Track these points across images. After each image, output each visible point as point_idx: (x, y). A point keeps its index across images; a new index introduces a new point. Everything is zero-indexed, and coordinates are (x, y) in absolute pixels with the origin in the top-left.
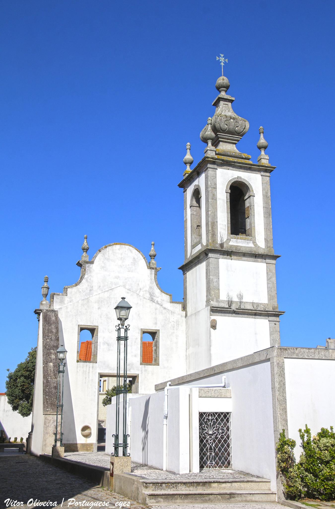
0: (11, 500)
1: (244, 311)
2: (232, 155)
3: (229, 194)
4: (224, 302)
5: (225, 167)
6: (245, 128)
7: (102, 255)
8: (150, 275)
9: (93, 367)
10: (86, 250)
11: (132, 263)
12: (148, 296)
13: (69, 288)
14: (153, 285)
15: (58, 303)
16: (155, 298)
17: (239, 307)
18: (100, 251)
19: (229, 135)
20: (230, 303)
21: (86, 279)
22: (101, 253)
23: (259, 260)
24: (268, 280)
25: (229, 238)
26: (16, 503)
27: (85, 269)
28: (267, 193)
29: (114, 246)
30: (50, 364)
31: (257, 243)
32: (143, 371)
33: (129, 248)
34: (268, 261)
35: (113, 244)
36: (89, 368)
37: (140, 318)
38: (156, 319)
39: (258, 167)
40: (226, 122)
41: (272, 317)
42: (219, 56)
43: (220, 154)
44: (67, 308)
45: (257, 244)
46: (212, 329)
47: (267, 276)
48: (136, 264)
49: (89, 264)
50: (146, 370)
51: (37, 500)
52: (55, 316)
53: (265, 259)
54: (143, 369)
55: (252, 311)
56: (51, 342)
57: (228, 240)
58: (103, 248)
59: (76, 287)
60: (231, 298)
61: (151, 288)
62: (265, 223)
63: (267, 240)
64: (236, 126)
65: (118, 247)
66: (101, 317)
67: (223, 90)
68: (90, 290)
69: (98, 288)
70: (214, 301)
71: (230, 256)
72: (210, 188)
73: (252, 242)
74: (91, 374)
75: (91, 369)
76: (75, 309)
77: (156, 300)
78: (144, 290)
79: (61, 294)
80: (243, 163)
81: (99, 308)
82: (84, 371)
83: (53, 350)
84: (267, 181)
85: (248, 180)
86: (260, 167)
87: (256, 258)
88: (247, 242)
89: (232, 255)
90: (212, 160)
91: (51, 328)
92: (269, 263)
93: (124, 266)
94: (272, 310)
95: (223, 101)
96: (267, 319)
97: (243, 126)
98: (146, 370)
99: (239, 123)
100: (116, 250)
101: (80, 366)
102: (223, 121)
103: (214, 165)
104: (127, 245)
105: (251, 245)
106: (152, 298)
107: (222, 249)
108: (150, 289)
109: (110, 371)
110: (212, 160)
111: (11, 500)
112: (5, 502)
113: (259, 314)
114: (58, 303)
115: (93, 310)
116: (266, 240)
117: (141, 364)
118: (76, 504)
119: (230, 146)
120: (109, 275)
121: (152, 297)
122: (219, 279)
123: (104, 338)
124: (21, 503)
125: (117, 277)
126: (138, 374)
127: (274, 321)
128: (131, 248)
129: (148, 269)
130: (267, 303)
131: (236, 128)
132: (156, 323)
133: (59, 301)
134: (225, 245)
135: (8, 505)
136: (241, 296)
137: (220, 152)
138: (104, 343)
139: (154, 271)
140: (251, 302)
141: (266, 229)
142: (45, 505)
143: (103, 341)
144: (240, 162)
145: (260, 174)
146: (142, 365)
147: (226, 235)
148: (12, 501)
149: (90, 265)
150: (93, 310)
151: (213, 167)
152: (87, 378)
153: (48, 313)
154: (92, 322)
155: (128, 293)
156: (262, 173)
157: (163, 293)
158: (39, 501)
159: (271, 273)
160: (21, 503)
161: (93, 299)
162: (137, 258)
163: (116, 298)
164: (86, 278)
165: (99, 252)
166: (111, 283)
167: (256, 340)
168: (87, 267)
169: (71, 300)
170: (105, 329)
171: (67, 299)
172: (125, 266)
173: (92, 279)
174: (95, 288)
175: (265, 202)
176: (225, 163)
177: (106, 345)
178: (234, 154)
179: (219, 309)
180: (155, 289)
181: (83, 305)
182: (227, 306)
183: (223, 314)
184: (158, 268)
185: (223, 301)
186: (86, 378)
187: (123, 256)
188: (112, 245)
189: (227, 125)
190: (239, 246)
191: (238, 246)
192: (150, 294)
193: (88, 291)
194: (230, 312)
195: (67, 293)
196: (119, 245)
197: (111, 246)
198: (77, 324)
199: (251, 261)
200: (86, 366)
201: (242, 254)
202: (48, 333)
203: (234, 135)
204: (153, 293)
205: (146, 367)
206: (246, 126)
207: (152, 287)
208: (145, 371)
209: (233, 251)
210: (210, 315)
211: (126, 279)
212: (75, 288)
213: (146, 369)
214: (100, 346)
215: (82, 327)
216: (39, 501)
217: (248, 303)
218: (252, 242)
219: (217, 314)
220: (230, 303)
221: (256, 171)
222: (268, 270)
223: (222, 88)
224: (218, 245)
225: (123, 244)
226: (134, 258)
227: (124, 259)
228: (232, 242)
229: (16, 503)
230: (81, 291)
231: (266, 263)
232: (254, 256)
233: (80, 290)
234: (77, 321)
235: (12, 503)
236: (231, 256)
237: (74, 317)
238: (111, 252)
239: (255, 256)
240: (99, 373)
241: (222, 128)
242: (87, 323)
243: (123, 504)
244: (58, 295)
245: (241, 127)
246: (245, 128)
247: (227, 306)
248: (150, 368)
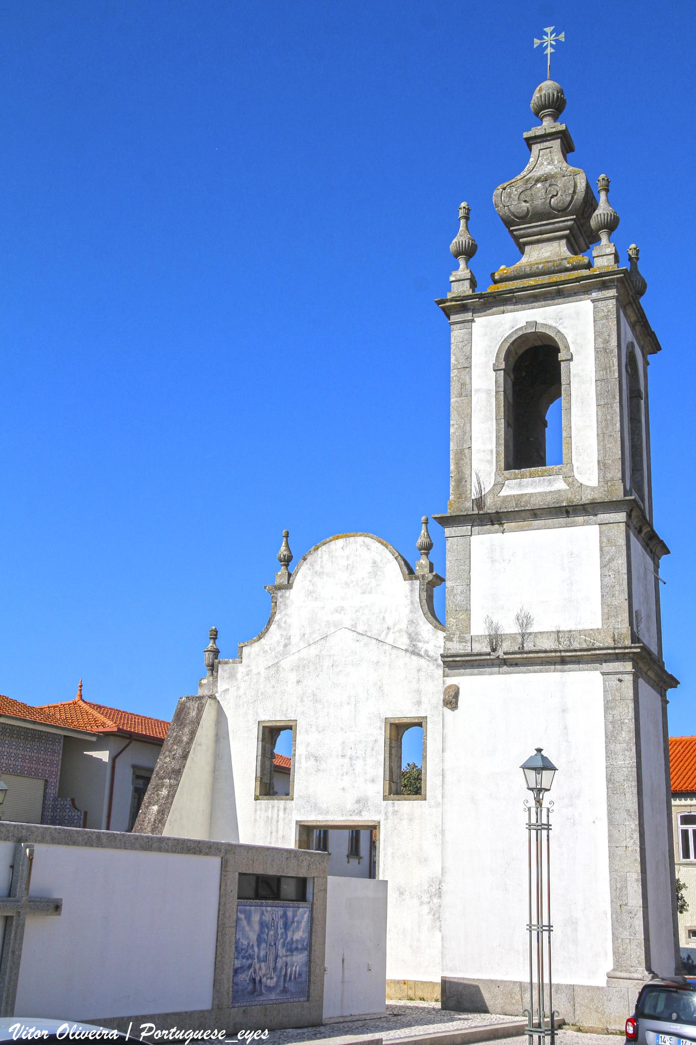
1: (525, 655)
2: (536, 272)
3: (502, 371)
4: (479, 641)
5: (495, 309)
6: (574, 192)
7: (309, 566)
8: (409, 594)
9: (285, 809)
10: (283, 561)
11: (370, 573)
12: (404, 642)
13: (246, 646)
14: (415, 615)
15: (225, 679)
16: (420, 645)
17: (519, 648)
18: (305, 559)
19: (539, 223)
20: (495, 640)
21: (277, 623)
22: (307, 564)
23: (580, 519)
24: (603, 566)
25: (500, 479)
27: (276, 603)
28: (607, 342)
29: (333, 543)
30: (153, 807)
31: (577, 476)
32: (390, 813)
33: (364, 542)
34: (602, 517)
35: (331, 538)
36: (278, 810)
37: (383, 694)
38: (419, 691)
39: (578, 284)
40: (522, 196)
41: (611, 664)
42: (541, 35)
43: (504, 278)
44: (238, 688)
45: (575, 480)
46: (447, 711)
47: (601, 557)
48: (379, 573)
49: (283, 591)
50: (395, 812)
52: (198, 710)
53: (596, 515)
54: (390, 809)
55: (548, 654)
56: (171, 763)
57: (499, 485)
58: (310, 552)
59: (259, 643)
60: (497, 629)
61: (411, 622)
62: (599, 420)
63: (605, 465)
64: (550, 196)
65: (340, 542)
66: (302, 701)
67: (543, 116)
68: (286, 646)
69: (300, 639)
70: (453, 641)
71: (498, 524)
72: (454, 371)
73: (561, 477)
74: (281, 823)
75: (281, 813)
76: (253, 689)
77: (423, 650)
78: (396, 629)
79: (231, 660)
80: (534, 287)
81: (298, 682)
82: (268, 817)
83: (170, 779)
84: (609, 311)
85: (554, 325)
86: (581, 282)
87: (568, 517)
88: (547, 481)
89: (503, 522)
90: (454, 303)
91: (182, 733)
92: (607, 522)
93: (352, 582)
94: (612, 645)
95: (540, 142)
96: (597, 669)
97: (569, 189)
98: (395, 812)
99: (556, 185)
100: (336, 550)
101: (261, 809)
102: (515, 195)
103: (466, 314)
104: (360, 536)
105: (559, 485)
106: (414, 646)
107: (481, 512)
108: (408, 626)
109: (319, 815)
110: (454, 303)
112: (10, 1030)
113: (574, 659)
114: (225, 679)
115: (287, 686)
116: (603, 465)
117: (385, 798)
119: (551, 248)
120: (323, 608)
121: (414, 643)
122: (469, 585)
123: (308, 745)
125: (339, 609)
126: (379, 822)
127: (616, 673)
128: (368, 540)
129: (405, 580)
130: (600, 627)
131: (553, 200)
132: (419, 703)
133: (227, 676)
134: (489, 501)
136: (524, 621)
137: (506, 273)
138: (308, 758)
139: (418, 582)
140: (553, 632)
141: (602, 436)
143: (307, 751)
144: (525, 287)
145: (589, 299)
146: (386, 802)
147: (493, 475)
148: (25, 1029)
149: (285, 592)
150: (287, 686)
151: (461, 320)
152: (274, 834)
153: (188, 704)
154: (284, 713)
155: (358, 641)
156: (594, 295)
157: (440, 630)
159: (614, 548)
160: (163, 1033)
161: (286, 663)
162: (381, 561)
163: (333, 655)
164: (278, 622)
165: (302, 561)
166: (326, 625)
167: (565, 728)
168: (279, 598)
169: (249, 671)
170: (311, 725)
171: (241, 669)
172: (354, 583)
173: (288, 621)
174: (294, 640)
175: (601, 367)
176: (491, 299)
177: (312, 759)
178: (541, 266)
179: (458, 659)
180: (421, 623)
181: (267, 678)
182: (488, 650)
183: (476, 671)
184: (427, 576)
185: (479, 638)
186: (272, 833)
187: (350, 562)
188: (328, 542)
189: (525, 201)
190: (526, 494)
191: (522, 494)
192: (409, 638)
193: (282, 648)
194: (493, 663)
195: (242, 658)
196: (342, 540)
197: (326, 543)
198: (256, 720)
199: (558, 526)
200: (273, 807)
201: (528, 513)
202: (172, 744)
203: (532, 223)
204: (417, 634)
205: (396, 805)
206: (578, 184)
207: (415, 621)
208: (393, 813)
209: (499, 512)
210: (444, 676)
211: (357, 611)
212: (256, 644)
213: (396, 810)
214: (301, 763)
215: (265, 725)
217: (545, 635)
218: (561, 477)
219: (462, 671)
220: (495, 640)
221: (578, 294)
222: (605, 540)
223: (541, 111)
224: (469, 504)
225: (352, 534)
226: (374, 562)
227: (353, 567)
228: (508, 489)
230: (267, 650)
231: (599, 524)
232: (562, 513)
233: (267, 648)
234: (257, 712)
235: (25, 1032)
236: (501, 524)
237: (252, 705)
238: (326, 557)
239: (564, 512)
240: (297, 822)
241: (516, 213)
242: (275, 716)
244: (226, 663)
245: (565, 192)
246: (574, 192)
247: (488, 650)
248: (407, 806)
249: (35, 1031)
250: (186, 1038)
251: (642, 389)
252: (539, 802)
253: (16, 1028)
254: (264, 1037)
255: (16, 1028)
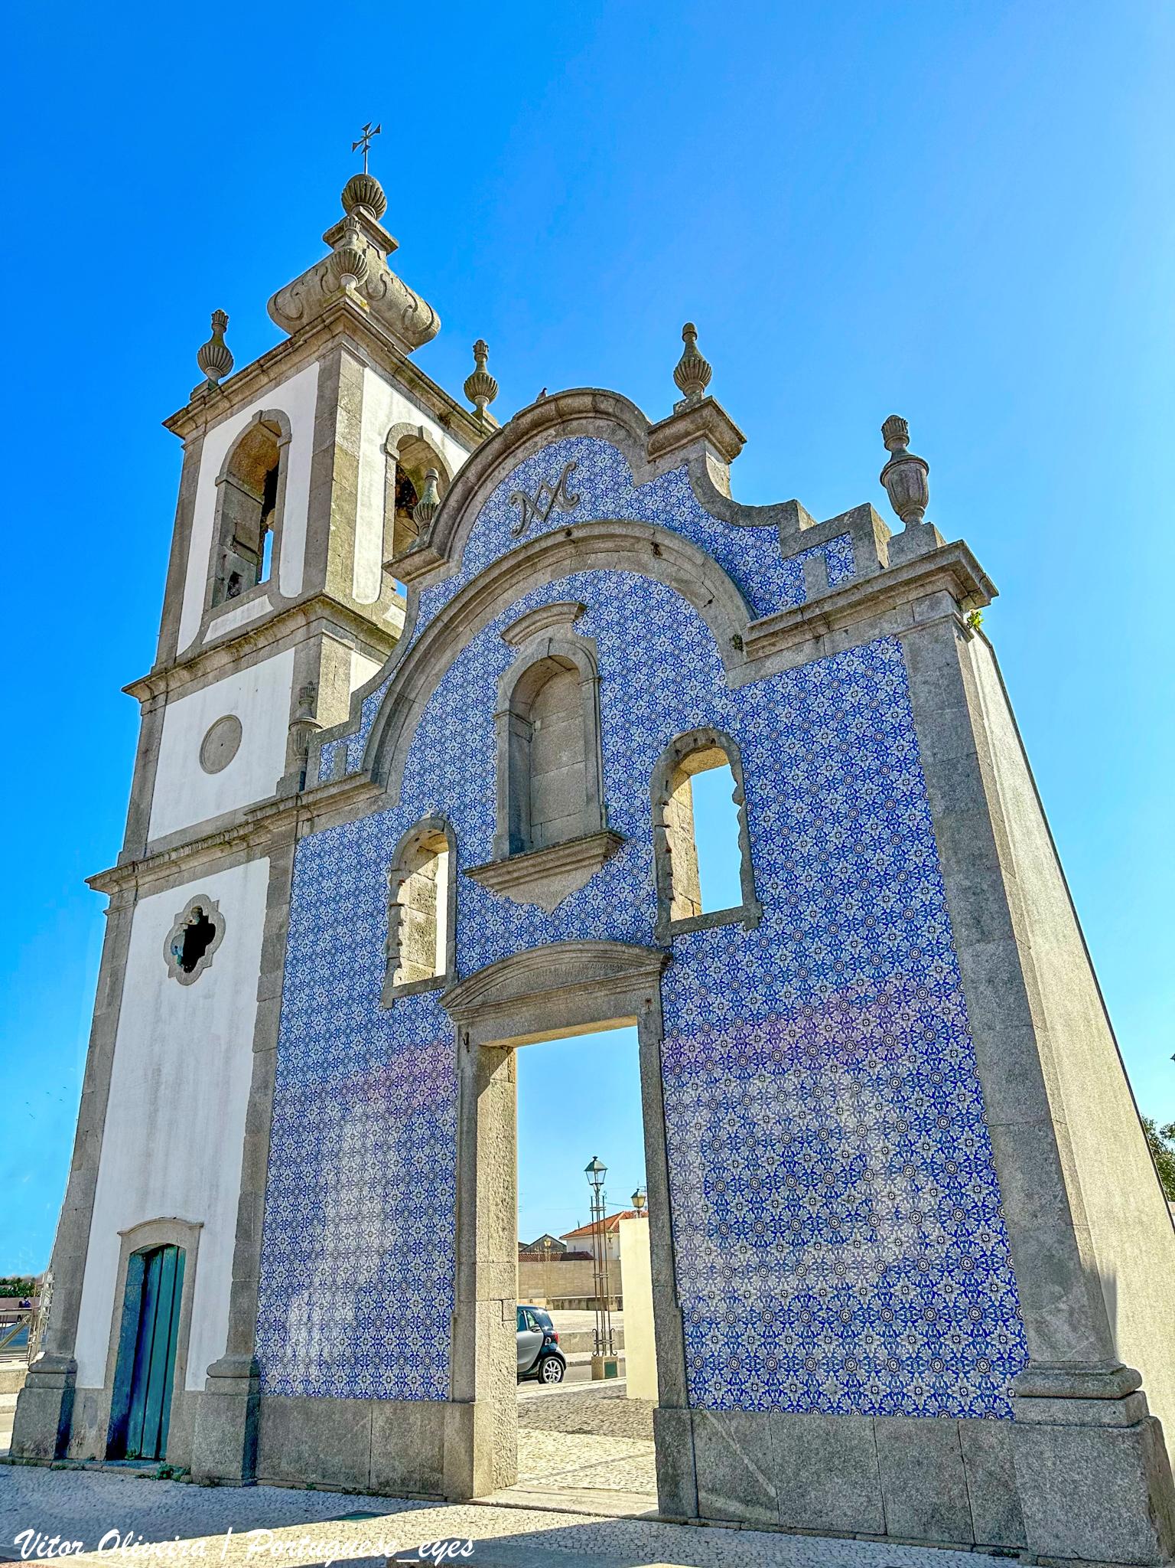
0: (40, 1534)
26: (56, 1547)
51: (131, 1534)
111: (40, 1534)
112: (17, 1540)
118: (65, 1548)
124: (76, 1544)
135: (26, 1552)
142: (453, 1552)
148: (42, 1539)
158: (140, 1538)
160: (74, 1546)
216: (140, 1538)
229: (56, 1547)
235: (43, 1544)
243: (447, 1549)
249: (60, 1543)
250: (434, 1554)
251: (593, 1519)
252: (597, 1192)
253: (26, 1537)
254: (465, 1554)
255: (26, 1537)
